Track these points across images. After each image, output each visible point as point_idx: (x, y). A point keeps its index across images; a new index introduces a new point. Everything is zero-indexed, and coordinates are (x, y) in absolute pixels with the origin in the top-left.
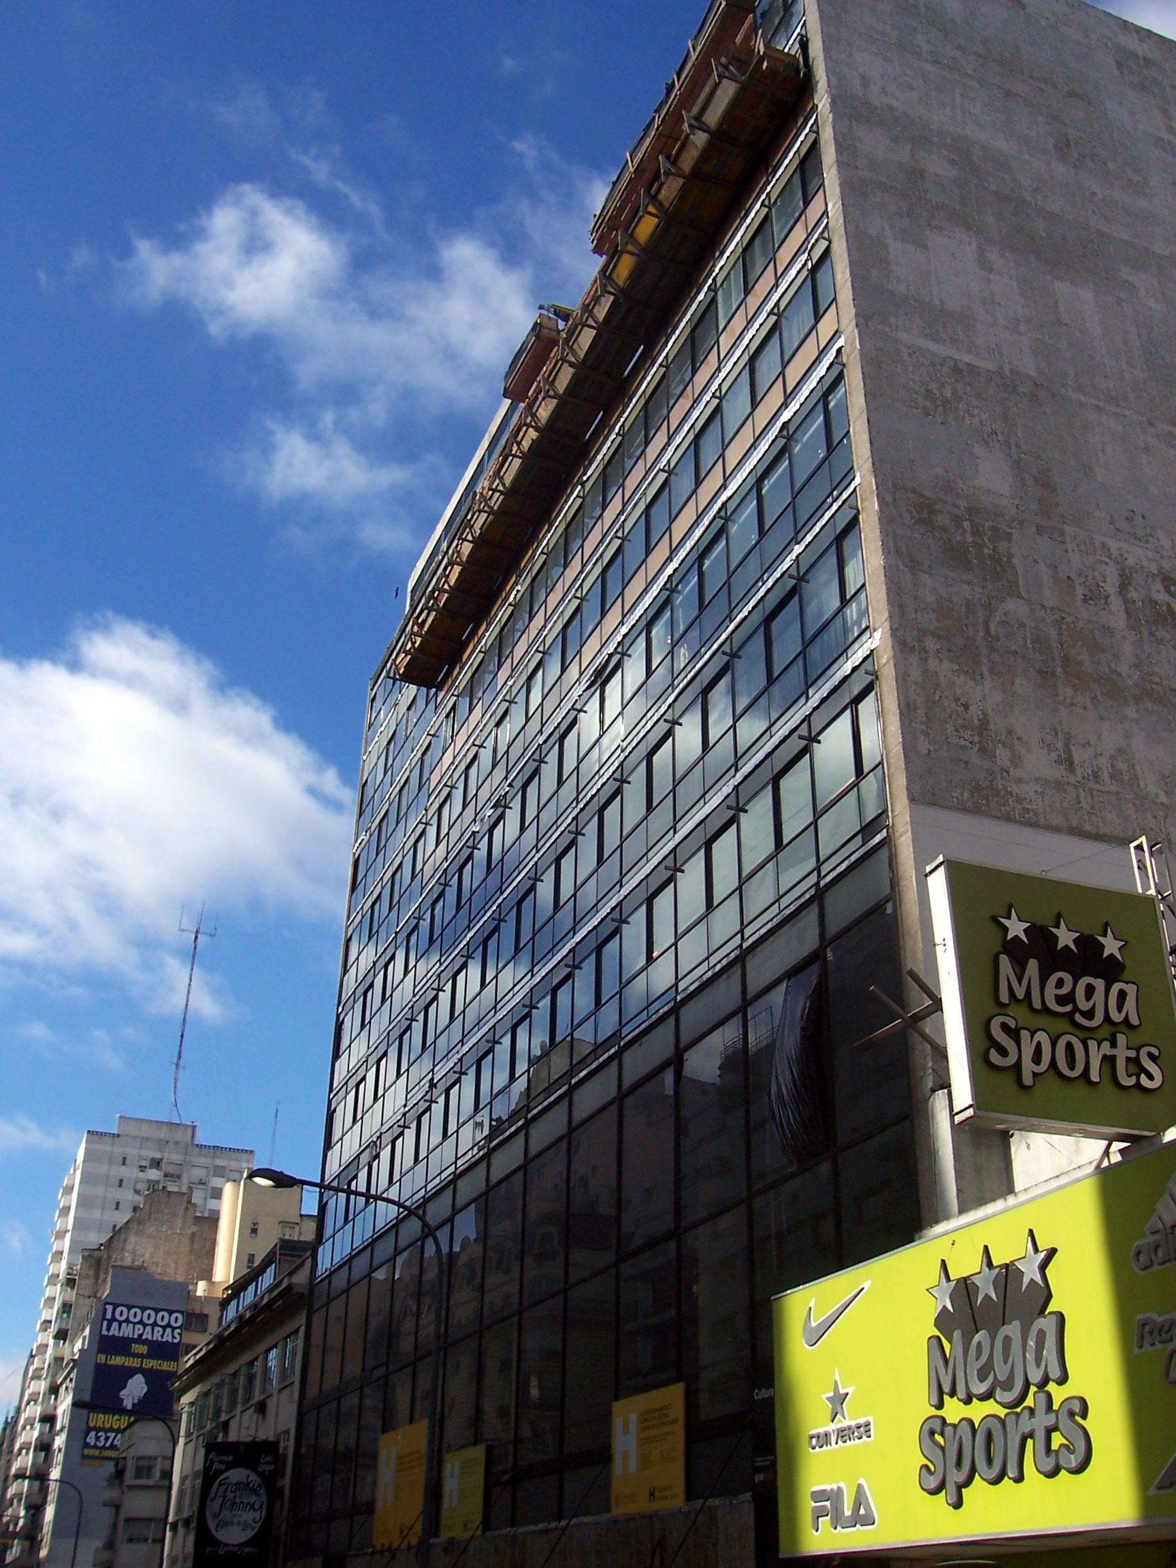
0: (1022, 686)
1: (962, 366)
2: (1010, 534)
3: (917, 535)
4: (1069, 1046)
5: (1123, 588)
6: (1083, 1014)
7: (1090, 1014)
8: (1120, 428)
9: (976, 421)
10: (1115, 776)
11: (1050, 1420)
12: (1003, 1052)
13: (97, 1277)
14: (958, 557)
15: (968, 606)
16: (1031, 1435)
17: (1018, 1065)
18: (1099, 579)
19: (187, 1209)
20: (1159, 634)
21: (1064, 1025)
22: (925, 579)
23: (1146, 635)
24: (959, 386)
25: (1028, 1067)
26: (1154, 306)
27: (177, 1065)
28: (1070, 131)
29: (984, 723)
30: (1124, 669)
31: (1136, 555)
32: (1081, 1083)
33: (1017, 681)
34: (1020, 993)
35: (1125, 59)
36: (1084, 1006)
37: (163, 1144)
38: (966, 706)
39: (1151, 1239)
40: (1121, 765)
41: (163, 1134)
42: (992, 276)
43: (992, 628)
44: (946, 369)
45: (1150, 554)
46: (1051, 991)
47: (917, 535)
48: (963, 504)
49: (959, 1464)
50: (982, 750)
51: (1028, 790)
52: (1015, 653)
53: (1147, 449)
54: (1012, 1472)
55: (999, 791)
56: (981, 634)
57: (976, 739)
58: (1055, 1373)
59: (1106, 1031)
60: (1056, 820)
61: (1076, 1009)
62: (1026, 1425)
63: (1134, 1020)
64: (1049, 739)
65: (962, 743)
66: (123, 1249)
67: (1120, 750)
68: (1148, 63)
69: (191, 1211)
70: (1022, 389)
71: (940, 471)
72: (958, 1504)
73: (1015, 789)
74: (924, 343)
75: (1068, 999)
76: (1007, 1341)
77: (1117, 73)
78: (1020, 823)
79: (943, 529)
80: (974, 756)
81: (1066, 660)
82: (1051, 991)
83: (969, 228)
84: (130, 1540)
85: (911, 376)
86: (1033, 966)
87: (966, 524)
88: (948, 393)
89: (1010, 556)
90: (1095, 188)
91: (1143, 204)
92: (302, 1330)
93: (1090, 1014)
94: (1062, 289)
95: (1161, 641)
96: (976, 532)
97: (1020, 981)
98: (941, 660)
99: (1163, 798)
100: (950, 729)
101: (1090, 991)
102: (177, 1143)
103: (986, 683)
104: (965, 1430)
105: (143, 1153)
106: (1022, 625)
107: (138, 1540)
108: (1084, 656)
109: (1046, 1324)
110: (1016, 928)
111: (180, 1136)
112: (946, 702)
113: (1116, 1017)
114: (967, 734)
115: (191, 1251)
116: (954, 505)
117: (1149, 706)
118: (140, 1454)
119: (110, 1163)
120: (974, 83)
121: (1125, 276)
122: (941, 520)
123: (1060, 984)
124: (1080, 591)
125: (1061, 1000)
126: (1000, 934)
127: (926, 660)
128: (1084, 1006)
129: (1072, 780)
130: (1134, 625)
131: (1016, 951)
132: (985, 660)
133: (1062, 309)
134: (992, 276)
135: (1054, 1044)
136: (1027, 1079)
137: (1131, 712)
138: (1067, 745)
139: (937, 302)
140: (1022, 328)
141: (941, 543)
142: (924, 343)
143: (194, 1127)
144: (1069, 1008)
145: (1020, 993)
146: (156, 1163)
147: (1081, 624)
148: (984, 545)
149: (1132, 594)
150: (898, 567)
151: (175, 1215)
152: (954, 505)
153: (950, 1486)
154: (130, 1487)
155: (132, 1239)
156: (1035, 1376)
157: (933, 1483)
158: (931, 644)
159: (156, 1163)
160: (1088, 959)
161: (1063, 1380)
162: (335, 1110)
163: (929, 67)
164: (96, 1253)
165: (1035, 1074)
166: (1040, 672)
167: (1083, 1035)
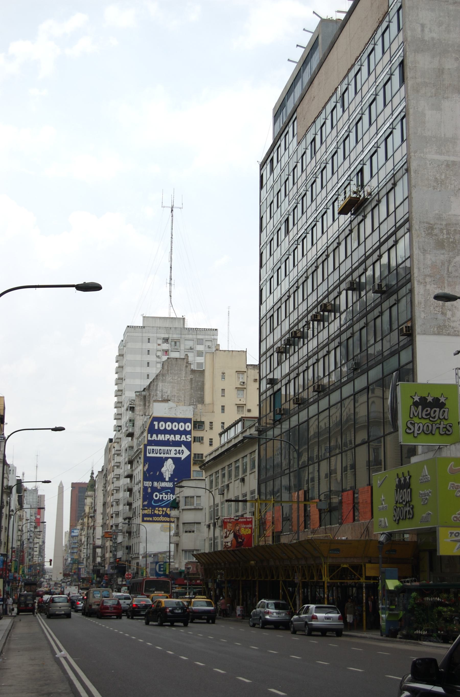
3: (426, 240)
6: (432, 418)
7: (435, 417)
9: (453, 186)
12: (410, 429)
13: (145, 405)
14: (440, 245)
15: (442, 263)
17: (414, 432)
19: (186, 366)
21: (427, 421)
24: (448, 172)
25: (416, 432)
27: (170, 284)
32: (431, 434)
34: (416, 414)
37: (168, 329)
41: (167, 324)
43: (450, 269)
44: (443, 166)
46: (424, 413)
47: (426, 240)
48: (444, 223)
50: (442, 313)
55: (446, 326)
56: (446, 272)
57: (440, 310)
59: (438, 421)
63: (446, 418)
65: (436, 312)
66: (156, 390)
69: (189, 367)
71: (437, 212)
72: (398, 523)
73: (452, 324)
75: (429, 414)
78: (453, 335)
79: (436, 235)
80: (440, 316)
82: (424, 413)
84: (186, 532)
85: (430, 174)
86: (420, 407)
88: (443, 177)
92: (257, 451)
93: (435, 417)
97: (416, 412)
98: (431, 285)
100: (432, 308)
102: (176, 328)
105: (159, 335)
107: (190, 532)
109: (409, 490)
111: (177, 325)
113: (441, 417)
115: (191, 388)
116: (441, 224)
118: (187, 495)
119: (142, 342)
122: (436, 231)
123: (427, 411)
127: (426, 286)
132: (446, 282)
136: (416, 435)
139: (443, 136)
141: (434, 241)
143: (184, 319)
144: (429, 416)
145: (416, 414)
146: (166, 340)
148: (450, 238)
150: (419, 253)
151: (181, 370)
152: (441, 224)
154: (183, 510)
155: (160, 384)
158: (428, 280)
159: (166, 340)
160: (438, 404)
161: (411, 501)
162: (262, 289)
164: (144, 393)
165: (418, 434)
167: (431, 423)
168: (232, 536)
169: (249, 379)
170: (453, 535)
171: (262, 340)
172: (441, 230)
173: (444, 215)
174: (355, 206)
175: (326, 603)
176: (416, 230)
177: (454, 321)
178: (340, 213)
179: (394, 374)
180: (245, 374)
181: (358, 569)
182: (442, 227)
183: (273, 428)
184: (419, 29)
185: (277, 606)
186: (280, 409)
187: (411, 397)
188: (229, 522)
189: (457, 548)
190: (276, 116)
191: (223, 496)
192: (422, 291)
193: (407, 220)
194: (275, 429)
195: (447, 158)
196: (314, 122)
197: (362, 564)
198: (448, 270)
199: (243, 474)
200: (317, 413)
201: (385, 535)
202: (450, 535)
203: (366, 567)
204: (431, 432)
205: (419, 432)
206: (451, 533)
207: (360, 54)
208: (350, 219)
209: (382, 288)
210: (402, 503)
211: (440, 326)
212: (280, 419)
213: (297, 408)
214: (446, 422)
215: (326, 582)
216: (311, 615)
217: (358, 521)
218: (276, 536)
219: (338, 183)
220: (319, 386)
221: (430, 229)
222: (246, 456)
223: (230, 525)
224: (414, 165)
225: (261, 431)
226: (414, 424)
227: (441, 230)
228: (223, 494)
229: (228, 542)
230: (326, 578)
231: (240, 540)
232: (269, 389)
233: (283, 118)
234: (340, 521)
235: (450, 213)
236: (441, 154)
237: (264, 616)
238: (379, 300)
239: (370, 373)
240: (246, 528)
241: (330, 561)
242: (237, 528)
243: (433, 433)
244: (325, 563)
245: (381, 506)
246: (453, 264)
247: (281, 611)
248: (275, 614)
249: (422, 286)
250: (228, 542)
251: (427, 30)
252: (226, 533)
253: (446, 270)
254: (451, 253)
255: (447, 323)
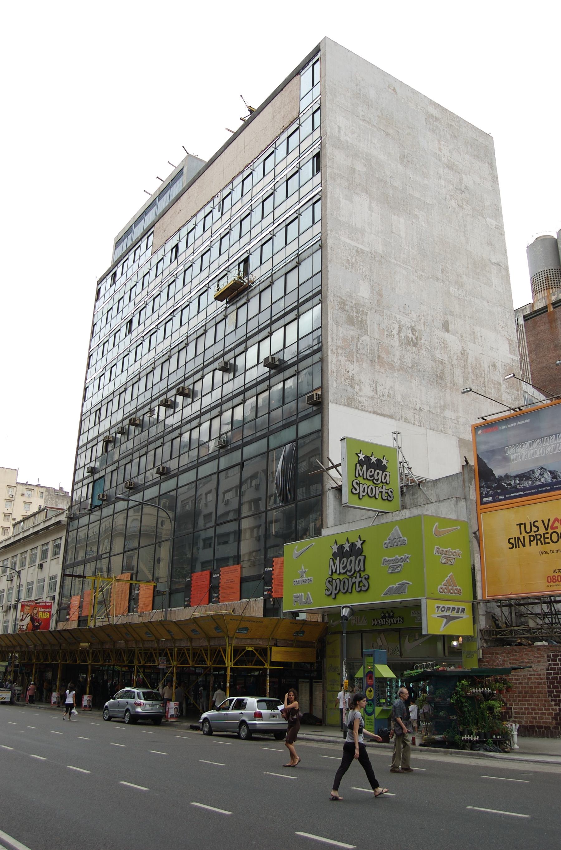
0: (365, 365)
1: (359, 250)
2: (367, 313)
4: (372, 488)
5: (399, 332)
7: (377, 480)
8: (406, 273)
9: (361, 271)
10: (389, 395)
11: (360, 579)
12: (356, 490)
14: (350, 321)
16: (355, 582)
17: (359, 493)
18: (392, 329)
20: (408, 348)
21: (371, 483)
22: (340, 328)
23: (404, 349)
24: (357, 257)
25: (361, 494)
26: (423, 225)
28: (406, 151)
29: (353, 377)
30: (396, 360)
31: (405, 321)
33: (364, 364)
34: (361, 474)
35: (430, 117)
36: (376, 478)
38: (348, 372)
39: (388, 541)
40: (391, 392)
42: (373, 214)
44: (354, 251)
45: (409, 320)
46: (369, 474)
48: (354, 302)
49: (336, 589)
50: (351, 386)
51: (362, 399)
52: (364, 354)
53: (413, 281)
54: (350, 591)
58: (362, 569)
59: (381, 485)
60: (370, 409)
61: (374, 479)
62: (354, 580)
63: (388, 482)
64: (371, 383)
67: (391, 387)
68: (436, 119)
70: (377, 259)
71: (348, 290)
73: (359, 399)
74: (349, 241)
76: (351, 561)
77: (425, 124)
79: (347, 311)
80: (349, 388)
81: (379, 356)
82: (369, 474)
83: (367, 194)
86: (365, 467)
87: (354, 309)
88: (354, 260)
89: (366, 321)
90: (411, 176)
91: (426, 182)
92: (64, 539)
93: (377, 480)
94: (395, 217)
95: (408, 351)
96: (357, 312)
97: (361, 471)
99: (402, 403)
100: (343, 379)
101: (378, 474)
103: (355, 364)
104: (338, 581)
106: (367, 345)
108: (385, 356)
109: (362, 558)
110: (362, 457)
112: (342, 370)
113: (384, 481)
114: (347, 381)
116: (351, 302)
117: (401, 372)
120: (376, 130)
121: (416, 213)
122: (347, 308)
123: (371, 472)
124: (386, 333)
125: (371, 476)
126: (357, 458)
128: (376, 478)
129: (376, 396)
130: (400, 346)
131: (360, 463)
133: (393, 227)
134: (373, 214)
135: (368, 488)
136: (361, 497)
137: (396, 375)
138: (376, 385)
139: (354, 225)
140: (380, 235)
142: (349, 241)
145: (361, 474)
147: (385, 345)
148: (359, 317)
149: (402, 335)
152: (351, 302)
153: (333, 594)
156: (357, 569)
157: (328, 593)
158: (340, 351)
160: (379, 466)
161: (364, 570)
163: (361, 123)
165: (363, 496)
166: (371, 361)
168: (28, 620)
169: (17, 493)
170: (440, 609)
171: (82, 433)
172: (352, 307)
173: (354, 295)
174: (235, 294)
175: (268, 695)
176: (331, 302)
177: (361, 396)
178: (217, 298)
179: (288, 447)
180: (15, 488)
181: (264, 652)
182: (351, 305)
183: (90, 514)
184: (337, 129)
185: (147, 696)
186: (103, 495)
187: (356, 454)
188: (27, 606)
189: (443, 625)
190: (118, 244)
191: (11, 583)
192: (335, 361)
193: (320, 292)
194: (91, 516)
195: (357, 245)
196: (179, 230)
197: (268, 647)
198: (357, 346)
199: (20, 567)
200: (195, 479)
201: (348, 609)
202: (437, 609)
203: (272, 650)
204: (375, 496)
205: (364, 494)
206: (438, 607)
207: (275, 139)
208: (225, 305)
209: (275, 362)
210: (345, 573)
211: (349, 398)
212: (101, 505)
213: (127, 493)
214: (388, 487)
215: (229, 668)
216: (254, 712)
217: (217, 602)
218: (82, 620)
219: (208, 276)
220: (130, 483)
221: (342, 304)
222: (17, 555)
223: (28, 608)
224: (330, 242)
225: (71, 518)
226: (359, 484)
227: (352, 307)
228: (12, 580)
229: (23, 626)
230: (230, 663)
231: (37, 624)
232: (87, 477)
233: (123, 247)
234: (186, 603)
235: (359, 294)
236: (352, 240)
237: (134, 708)
238: (268, 374)
239: (245, 449)
240: (44, 612)
241: (234, 642)
242: (35, 612)
243: (377, 497)
244: (229, 644)
245: (300, 579)
246: (360, 342)
247: (154, 702)
248: (148, 706)
249: (334, 356)
250: (23, 626)
251: (342, 133)
252: (23, 616)
253: (355, 346)
254: (359, 331)
255: (355, 397)
